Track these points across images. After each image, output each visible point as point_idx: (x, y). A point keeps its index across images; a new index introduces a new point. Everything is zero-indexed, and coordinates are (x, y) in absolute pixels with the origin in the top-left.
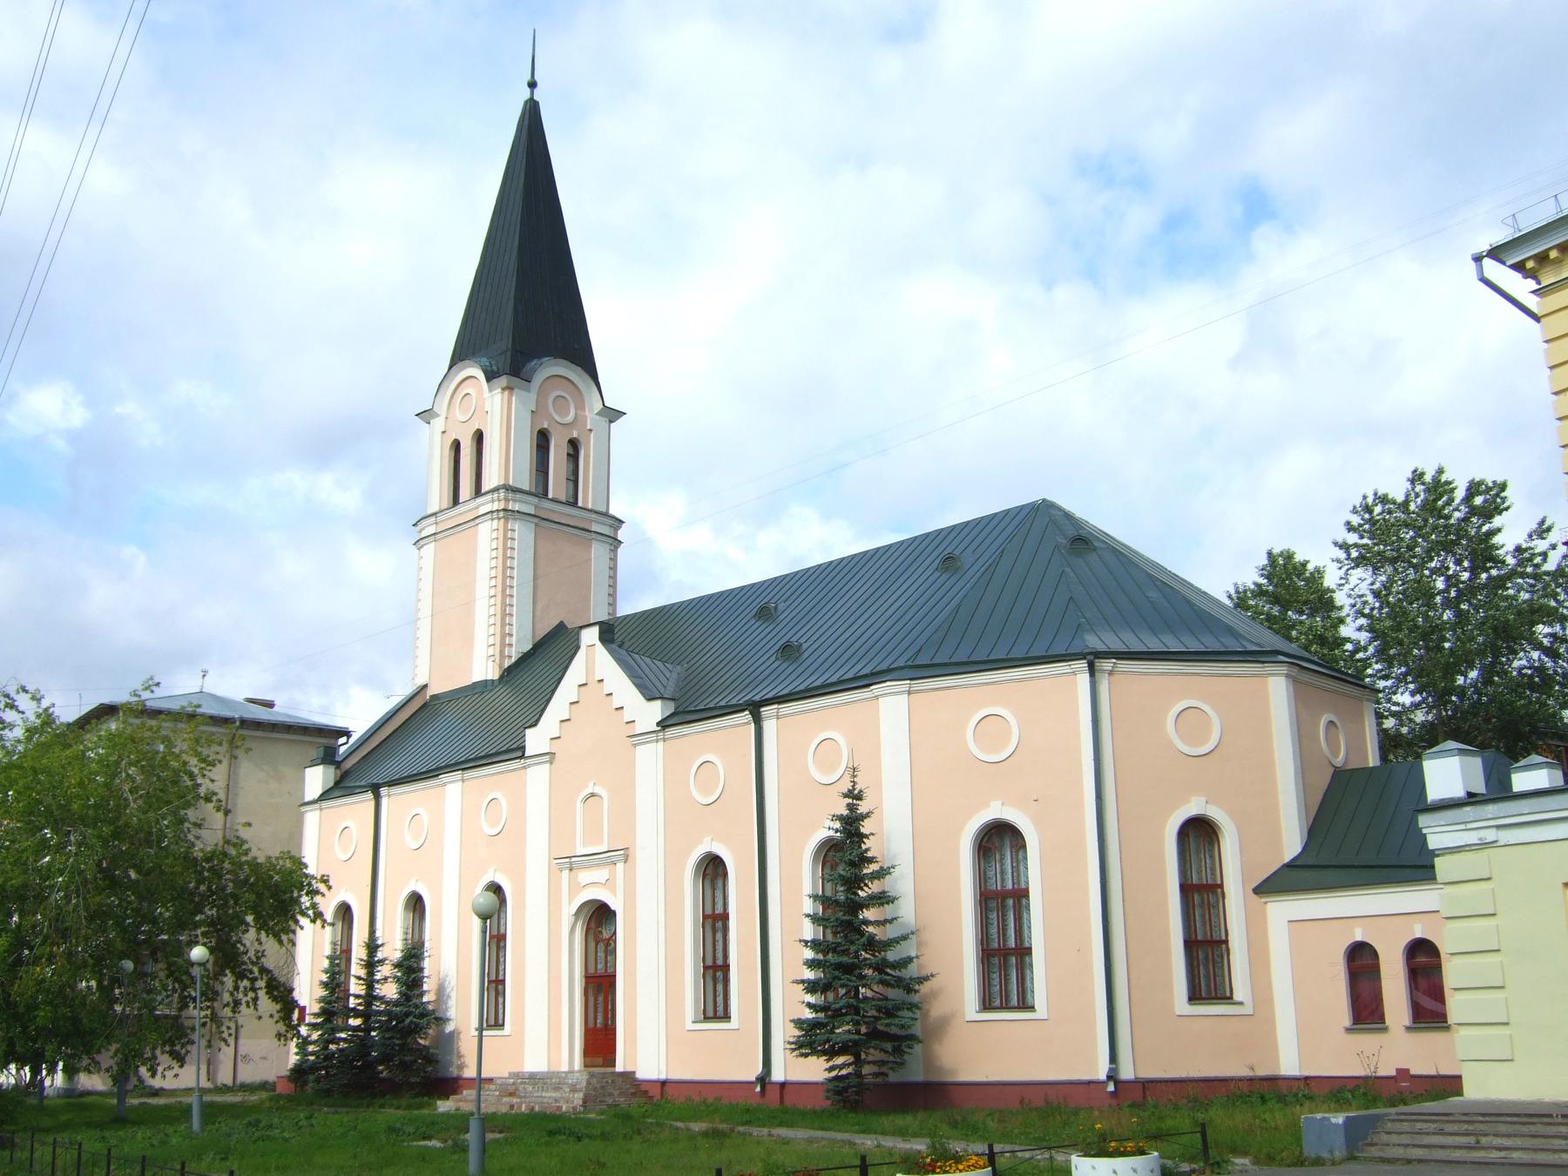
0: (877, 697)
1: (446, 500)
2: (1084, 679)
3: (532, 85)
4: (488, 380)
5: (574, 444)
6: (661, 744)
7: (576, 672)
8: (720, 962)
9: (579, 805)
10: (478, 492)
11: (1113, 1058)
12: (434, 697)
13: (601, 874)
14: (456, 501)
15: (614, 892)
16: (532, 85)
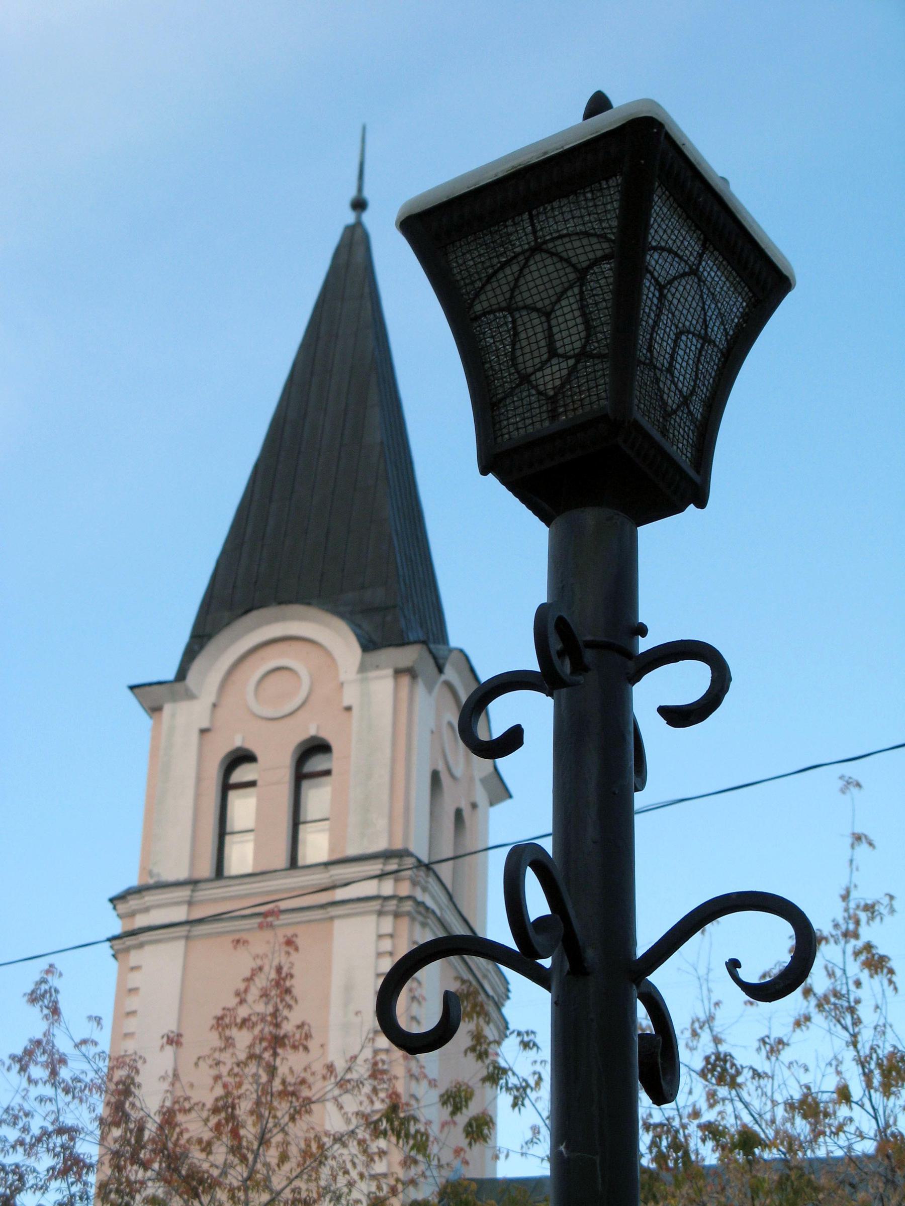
3: (359, 205)
5: (459, 814)
16: (359, 205)
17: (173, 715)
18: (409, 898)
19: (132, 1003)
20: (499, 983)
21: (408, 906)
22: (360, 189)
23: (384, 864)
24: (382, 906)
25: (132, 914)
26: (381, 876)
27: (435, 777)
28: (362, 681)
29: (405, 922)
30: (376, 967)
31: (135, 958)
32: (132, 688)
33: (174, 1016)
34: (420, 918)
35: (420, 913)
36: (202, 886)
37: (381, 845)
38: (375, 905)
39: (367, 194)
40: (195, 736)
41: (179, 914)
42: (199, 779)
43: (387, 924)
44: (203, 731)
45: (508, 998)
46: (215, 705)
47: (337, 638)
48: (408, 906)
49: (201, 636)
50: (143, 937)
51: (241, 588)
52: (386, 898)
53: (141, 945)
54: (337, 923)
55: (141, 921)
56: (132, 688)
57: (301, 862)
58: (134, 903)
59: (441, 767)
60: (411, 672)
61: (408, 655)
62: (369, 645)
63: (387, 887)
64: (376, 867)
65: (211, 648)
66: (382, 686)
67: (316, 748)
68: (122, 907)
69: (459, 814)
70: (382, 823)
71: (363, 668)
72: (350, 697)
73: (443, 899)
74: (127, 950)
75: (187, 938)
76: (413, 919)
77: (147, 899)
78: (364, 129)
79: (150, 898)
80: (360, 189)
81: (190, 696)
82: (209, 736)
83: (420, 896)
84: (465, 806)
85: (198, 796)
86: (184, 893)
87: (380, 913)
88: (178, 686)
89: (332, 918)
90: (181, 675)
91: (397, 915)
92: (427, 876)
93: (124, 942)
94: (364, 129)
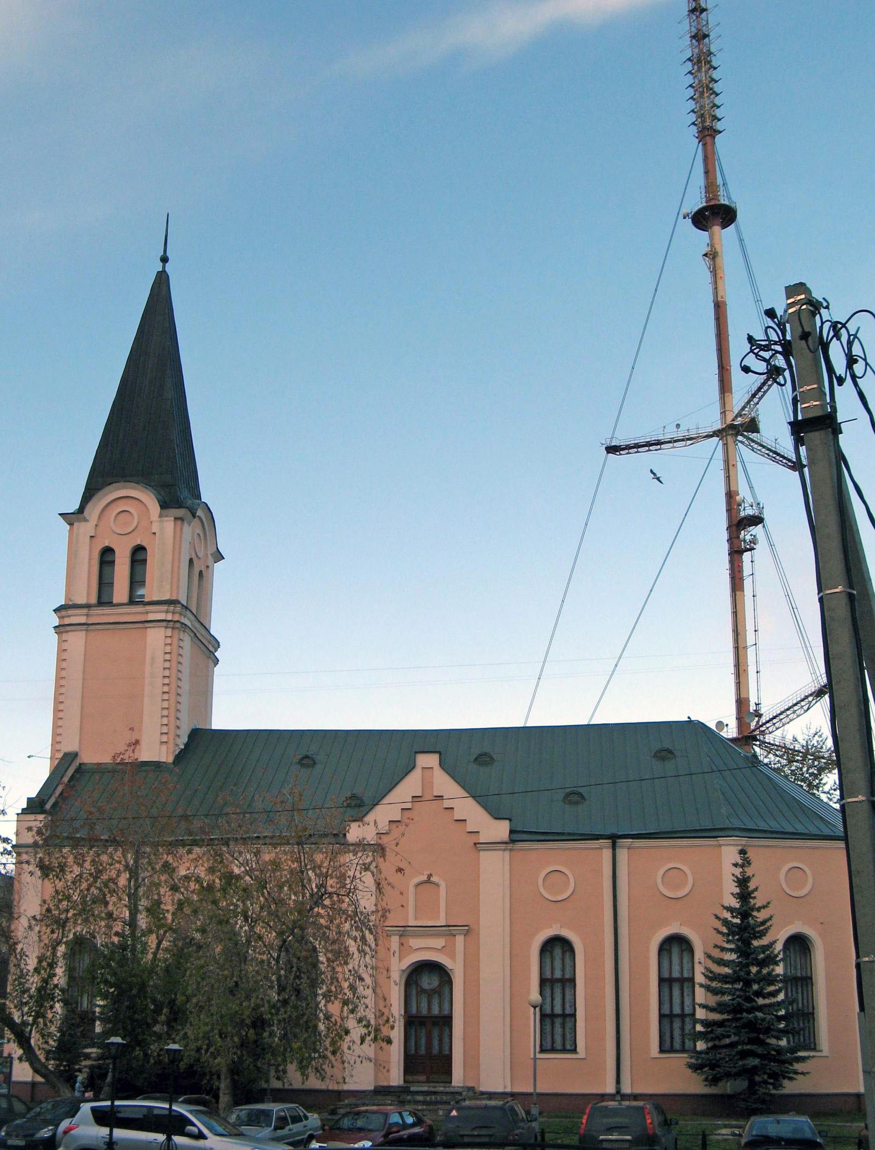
0: (720, 846)
1: (94, 600)
2: (607, 854)
3: (164, 260)
5: (201, 573)
6: (507, 853)
7: (409, 787)
8: (568, 1011)
9: (412, 889)
11: (618, 1081)
13: (439, 942)
14: (104, 599)
15: (453, 956)
16: (164, 260)
17: (78, 528)
19: (65, 656)
21: (178, 625)
26: (167, 612)
27: (191, 561)
29: (176, 632)
31: (65, 636)
32: (60, 514)
37: (166, 597)
38: (164, 624)
40: (88, 539)
41: (83, 620)
43: (169, 632)
44: (91, 537)
45: (219, 556)
47: (150, 500)
50: (68, 628)
51: (106, 472)
53: (67, 632)
54: (148, 630)
55: (67, 621)
56: (60, 514)
58: (64, 613)
59: (194, 557)
60: (182, 519)
61: (180, 512)
62: (164, 505)
63: (169, 617)
64: (165, 608)
65: (95, 499)
66: (169, 525)
69: (201, 573)
70: (168, 587)
71: (161, 516)
73: (193, 618)
74: (62, 633)
79: (70, 612)
81: (86, 520)
83: (183, 620)
84: (203, 568)
85: (89, 586)
86: (85, 611)
87: (166, 627)
88: (80, 516)
90: (81, 510)
91: (173, 628)
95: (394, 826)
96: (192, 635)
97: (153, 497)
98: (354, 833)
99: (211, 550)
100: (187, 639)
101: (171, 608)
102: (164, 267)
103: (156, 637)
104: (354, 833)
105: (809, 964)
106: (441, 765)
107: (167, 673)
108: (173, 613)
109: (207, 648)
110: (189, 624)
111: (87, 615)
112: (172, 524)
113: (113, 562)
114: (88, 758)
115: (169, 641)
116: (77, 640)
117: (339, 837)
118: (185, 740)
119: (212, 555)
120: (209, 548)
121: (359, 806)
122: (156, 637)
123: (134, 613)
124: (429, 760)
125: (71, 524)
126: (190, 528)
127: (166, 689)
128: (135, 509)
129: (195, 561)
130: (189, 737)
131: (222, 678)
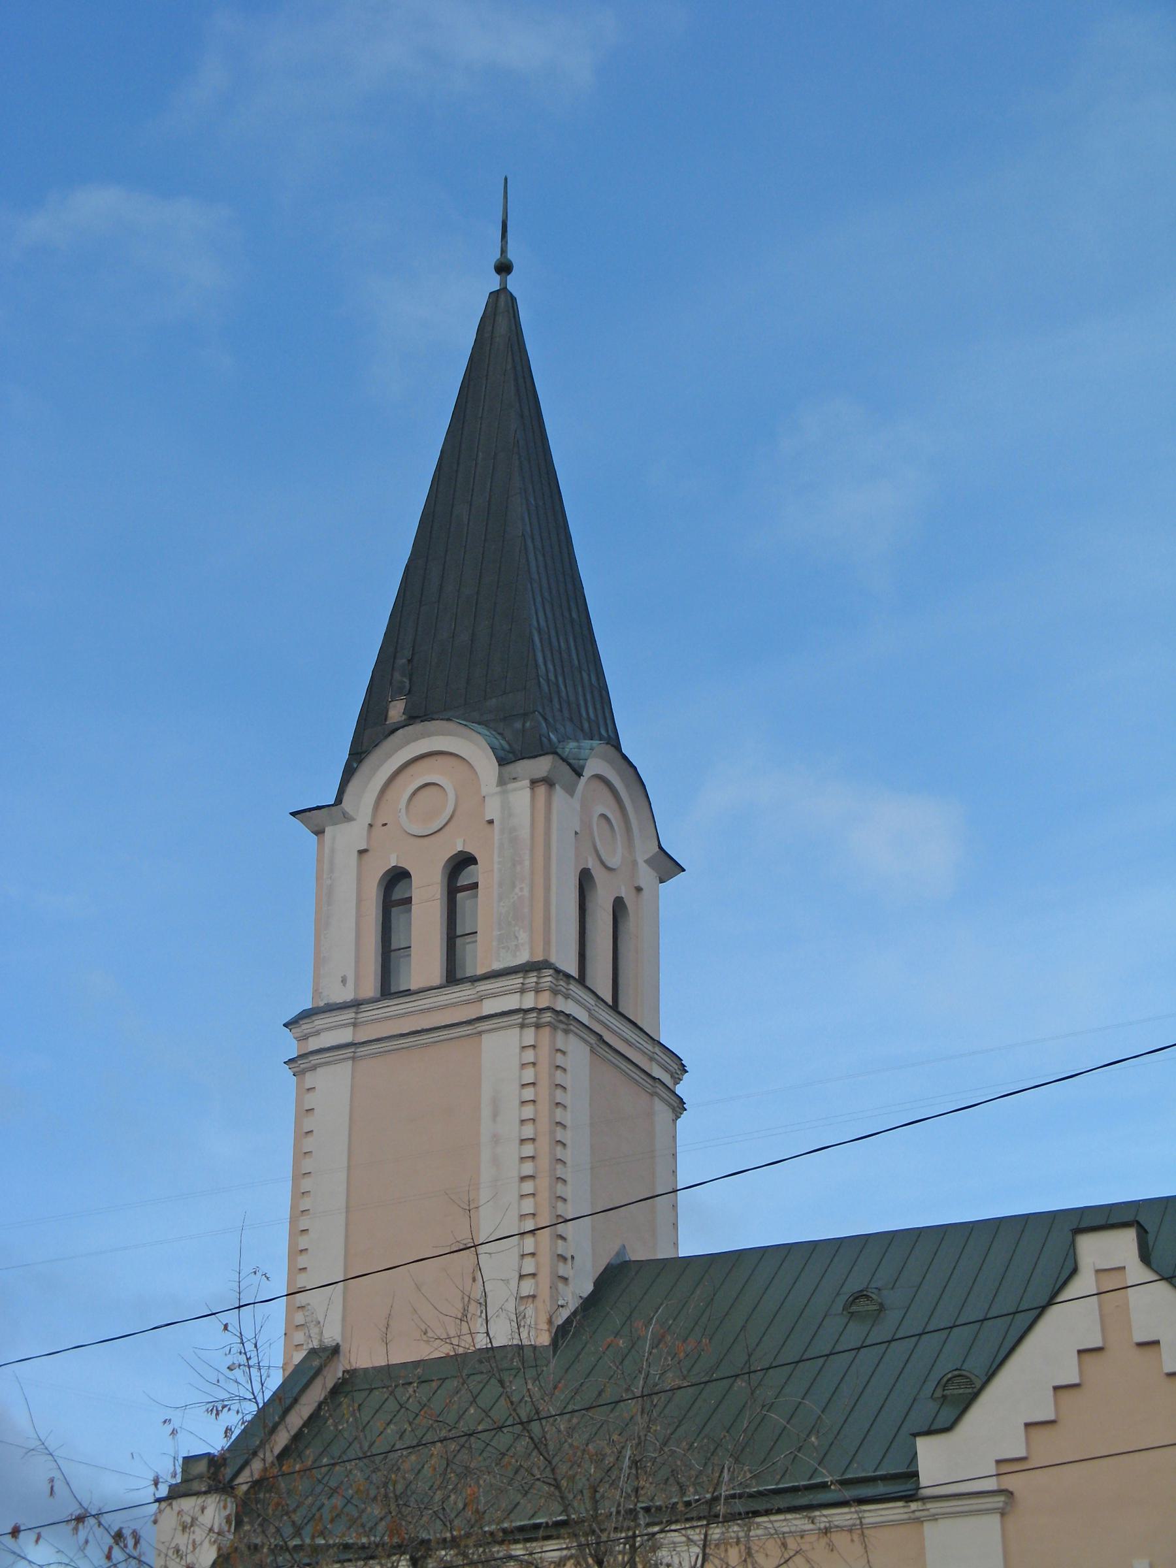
1: (370, 988)
4: (502, 762)
5: (619, 906)
10: (453, 977)
12: (351, 1376)
14: (387, 990)
16: (503, 268)
18: (548, 1008)
20: (669, 1061)
21: (547, 1017)
22: (504, 251)
23: (524, 978)
24: (524, 1019)
25: (304, 1038)
26: (522, 991)
27: (585, 880)
28: (504, 792)
30: (520, 1078)
31: (310, 1079)
32: (293, 814)
33: (510, 1032)
34: (562, 1026)
35: (561, 1021)
36: (363, 1008)
37: (523, 958)
38: (517, 1018)
39: (511, 255)
41: (345, 1036)
42: (359, 901)
43: (529, 1036)
44: (362, 852)
46: (371, 825)
47: (473, 748)
48: (547, 1017)
49: (359, 753)
50: (315, 1060)
52: (526, 1011)
53: (314, 1068)
55: (314, 1044)
56: (293, 814)
57: (459, 976)
58: (306, 1027)
60: (548, 782)
61: (542, 765)
63: (529, 1001)
64: (516, 981)
66: (521, 796)
67: (463, 861)
68: (298, 1031)
71: (501, 782)
72: (492, 810)
75: (353, 1058)
76: (555, 1028)
77: (317, 1023)
78: (506, 179)
79: (319, 1022)
80: (504, 251)
81: (347, 818)
82: (366, 856)
83: (570, 1007)
86: (349, 1015)
87: (522, 1026)
89: (480, 1033)
90: (339, 800)
91: (538, 1026)
92: (568, 984)
93: (300, 1064)
94: (506, 179)
95: (1039, 1434)
96: (592, 1040)
97: (484, 744)
98: (935, 1460)
99: (644, 850)
100: (577, 1051)
101: (532, 979)
102: (504, 283)
103: (503, 1053)
104: (935, 1460)
105: (607, 711)
106: (1145, 1257)
107: (528, 1131)
108: (537, 991)
109: (657, 1078)
110: (583, 1016)
111: (355, 1025)
112: (527, 793)
113: (408, 901)
114: (364, 1355)
115: (529, 1056)
116: (334, 1083)
117: (904, 1485)
118: (587, 1288)
119: (646, 861)
120: (637, 842)
121: (956, 1397)
122: (503, 1053)
123: (456, 1004)
124: (1122, 1247)
125: (319, 832)
126: (575, 803)
127: (528, 1169)
128: (459, 781)
129: (598, 874)
130: (596, 1284)
131: (699, 1145)
